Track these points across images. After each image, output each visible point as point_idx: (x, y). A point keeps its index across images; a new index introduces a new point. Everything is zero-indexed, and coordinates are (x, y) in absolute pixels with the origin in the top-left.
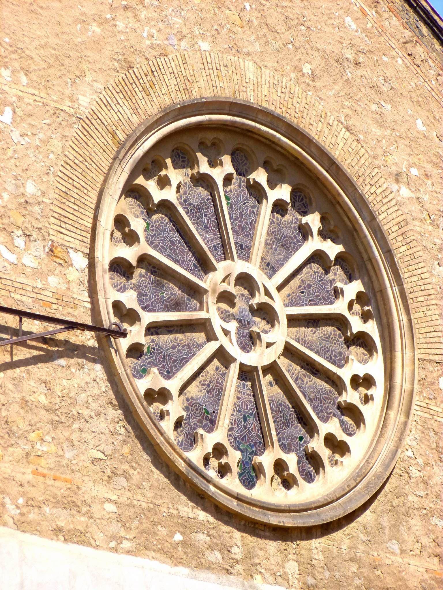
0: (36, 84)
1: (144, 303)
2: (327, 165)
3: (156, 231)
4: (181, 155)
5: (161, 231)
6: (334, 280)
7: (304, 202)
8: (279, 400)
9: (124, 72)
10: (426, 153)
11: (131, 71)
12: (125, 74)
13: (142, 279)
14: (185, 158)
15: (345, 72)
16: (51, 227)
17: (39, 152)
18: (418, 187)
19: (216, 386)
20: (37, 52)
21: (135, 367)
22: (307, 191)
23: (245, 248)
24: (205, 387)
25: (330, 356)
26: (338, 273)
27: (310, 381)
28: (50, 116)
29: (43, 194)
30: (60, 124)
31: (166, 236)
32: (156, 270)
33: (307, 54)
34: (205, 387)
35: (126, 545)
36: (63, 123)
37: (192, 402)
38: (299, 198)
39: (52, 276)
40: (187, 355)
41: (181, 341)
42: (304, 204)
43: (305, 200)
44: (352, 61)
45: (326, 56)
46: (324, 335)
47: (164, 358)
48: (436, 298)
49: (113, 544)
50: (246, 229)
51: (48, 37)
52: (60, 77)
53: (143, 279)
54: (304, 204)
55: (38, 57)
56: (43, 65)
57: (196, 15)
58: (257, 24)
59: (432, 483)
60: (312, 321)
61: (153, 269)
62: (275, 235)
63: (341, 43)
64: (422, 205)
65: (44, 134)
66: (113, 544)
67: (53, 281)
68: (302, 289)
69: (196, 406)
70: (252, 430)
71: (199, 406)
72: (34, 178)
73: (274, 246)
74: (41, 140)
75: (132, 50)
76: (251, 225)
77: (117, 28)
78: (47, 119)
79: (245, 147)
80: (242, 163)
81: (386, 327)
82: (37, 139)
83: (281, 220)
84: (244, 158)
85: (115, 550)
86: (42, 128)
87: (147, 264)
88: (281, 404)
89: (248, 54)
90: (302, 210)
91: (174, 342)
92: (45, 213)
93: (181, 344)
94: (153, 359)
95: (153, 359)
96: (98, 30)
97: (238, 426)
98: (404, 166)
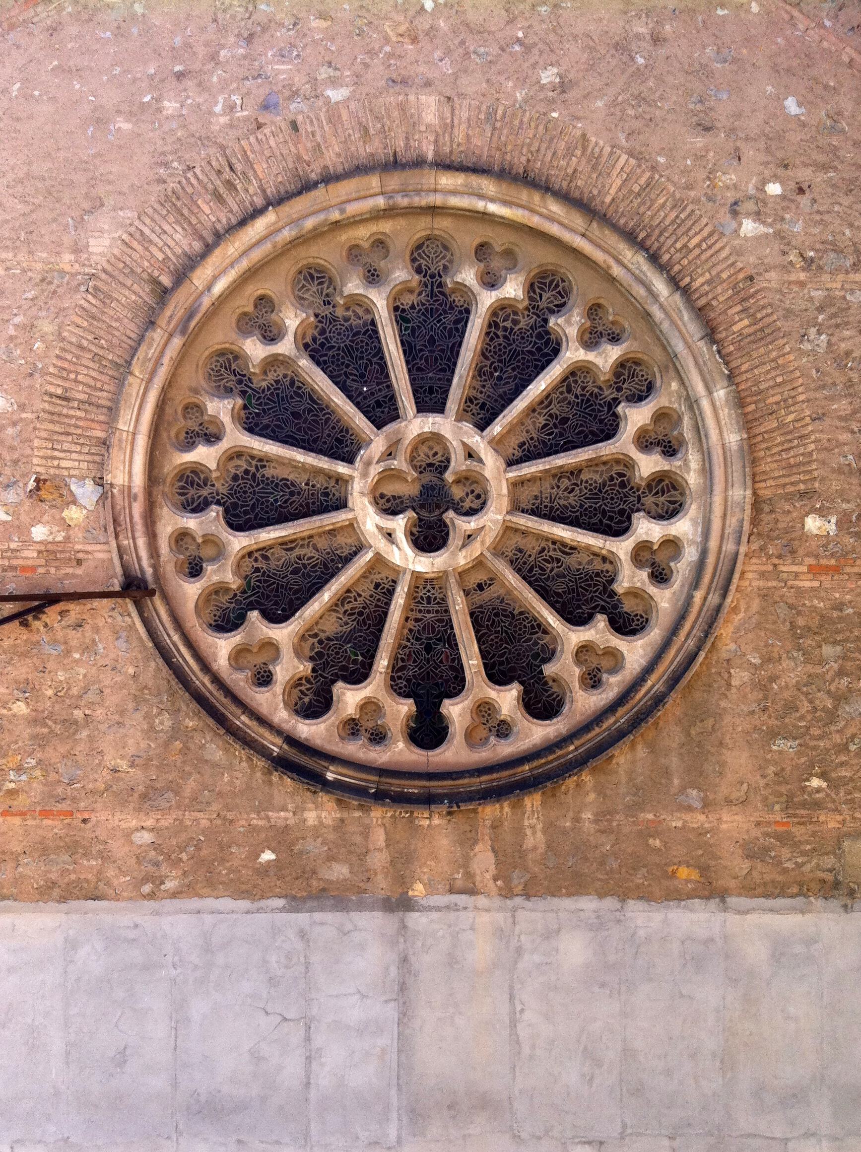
0: (9, 243)
1: (241, 517)
2: (582, 224)
3: (266, 404)
4: (316, 275)
5: (275, 403)
6: (615, 399)
7: (560, 288)
8: (494, 609)
9: (177, 180)
10: (801, 151)
11: (190, 175)
12: (179, 182)
13: (237, 484)
14: (323, 277)
15: (195, 203)
16: (36, 453)
17: (15, 346)
18: (780, 213)
19: (375, 612)
20: (10, 191)
21: (225, 614)
22: (562, 270)
23: (437, 391)
24: (354, 617)
25: (601, 521)
26: (624, 386)
27: (558, 567)
28: (37, 285)
29: (22, 407)
30: (55, 292)
31: (284, 408)
32: (265, 463)
33: (552, 51)
34: (354, 617)
35: (170, 885)
36: (59, 290)
37: (327, 644)
38: (550, 286)
39: (38, 526)
40: (320, 578)
41: (309, 559)
42: (559, 293)
43: (561, 285)
44: (648, 37)
45: (591, 43)
46: (591, 490)
47: (277, 591)
48: (808, 390)
49: (147, 888)
50: (441, 359)
51: (30, 164)
52: (55, 220)
53: (240, 482)
54: (559, 293)
55: (11, 199)
56: (26, 209)
57: (321, 49)
58: (446, 29)
59: (776, 687)
60: (568, 474)
61: (259, 464)
62: (500, 356)
63: (626, 13)
64: (786, 241)
65: (24, 315)
66: (147, 888)
67: (39, 532)
68: (551, 428)
69: (336, 648)
70: (441, 662)
71: (340, 649)
72: (5, 386)
73: (496, 374)
74: (16, 326)
75: (193, 140)
76: (452, 352)
77: (165, 113)
78: (30, 291)
79: (437, 232)
80: (437, 257)
81: (706, 454)
82: (11, 327)
83: (512, 329)
84: (441, 249)
85: (151, 896)
86: (19, 307)
87: (248, 458)
88: (497, 615)
89: (428, 84)
90: (556, 303)
91: (297, 563)
92: (25, 435)
93: (309, 564)
94: (258, 597)
95: (258, 597)
96: (126, 126)
97: (415, 661)
98: (751, 186)
